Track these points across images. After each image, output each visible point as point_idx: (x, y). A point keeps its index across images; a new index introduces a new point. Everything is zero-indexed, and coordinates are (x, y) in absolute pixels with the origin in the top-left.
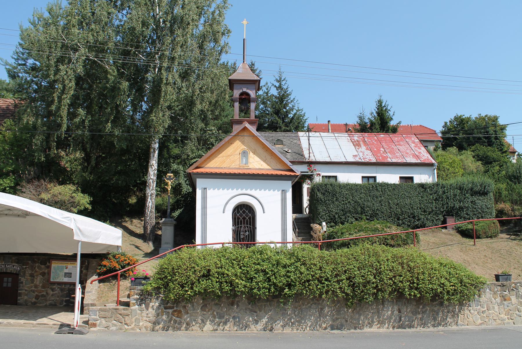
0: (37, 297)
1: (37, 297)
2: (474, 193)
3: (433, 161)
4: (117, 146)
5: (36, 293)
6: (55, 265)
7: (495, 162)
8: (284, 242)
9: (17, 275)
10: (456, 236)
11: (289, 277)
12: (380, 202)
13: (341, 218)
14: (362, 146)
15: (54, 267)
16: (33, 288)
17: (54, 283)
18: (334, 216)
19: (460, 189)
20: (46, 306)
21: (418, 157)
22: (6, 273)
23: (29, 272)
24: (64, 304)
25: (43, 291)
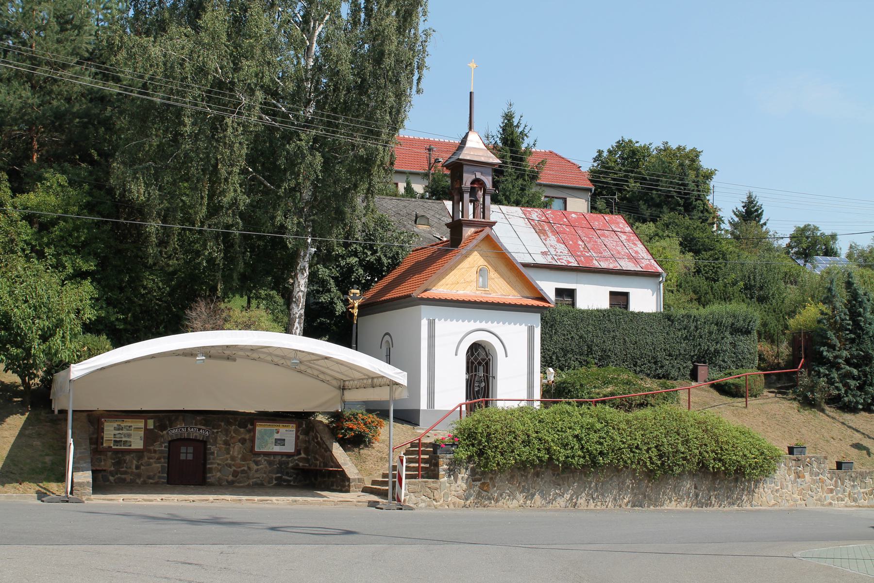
0: (235, 474)
1: (235, 474)
2: (736, 330)
3: (660, 270)
4: (290, 246)
5: (234, 468)
6: (261, 428)
7: (705, 250)
8: (530, 401)
9: (204, 442)
10: (708, 391)
11: (601, 444)
12: (614, 338)
13: (559, 361)
14: (550, 234)
15: (260, 431)
16: (229, 461)
17: (259, 454)
18: (551, 358)
19: (717, 324)
20: (248, 486)
21: (635, 260)
22: (189, 440)
23: (221, 438)
24: (275, 482)
25: (243, 466)
